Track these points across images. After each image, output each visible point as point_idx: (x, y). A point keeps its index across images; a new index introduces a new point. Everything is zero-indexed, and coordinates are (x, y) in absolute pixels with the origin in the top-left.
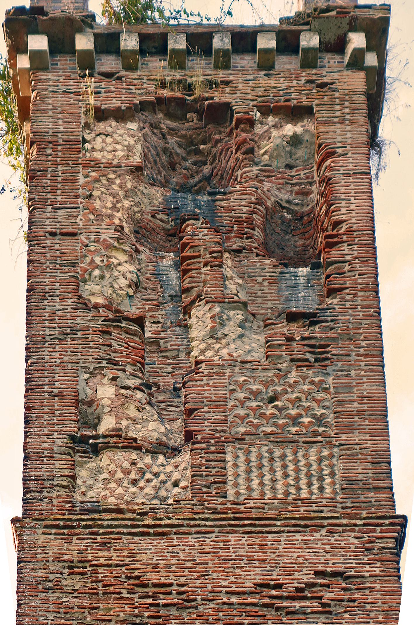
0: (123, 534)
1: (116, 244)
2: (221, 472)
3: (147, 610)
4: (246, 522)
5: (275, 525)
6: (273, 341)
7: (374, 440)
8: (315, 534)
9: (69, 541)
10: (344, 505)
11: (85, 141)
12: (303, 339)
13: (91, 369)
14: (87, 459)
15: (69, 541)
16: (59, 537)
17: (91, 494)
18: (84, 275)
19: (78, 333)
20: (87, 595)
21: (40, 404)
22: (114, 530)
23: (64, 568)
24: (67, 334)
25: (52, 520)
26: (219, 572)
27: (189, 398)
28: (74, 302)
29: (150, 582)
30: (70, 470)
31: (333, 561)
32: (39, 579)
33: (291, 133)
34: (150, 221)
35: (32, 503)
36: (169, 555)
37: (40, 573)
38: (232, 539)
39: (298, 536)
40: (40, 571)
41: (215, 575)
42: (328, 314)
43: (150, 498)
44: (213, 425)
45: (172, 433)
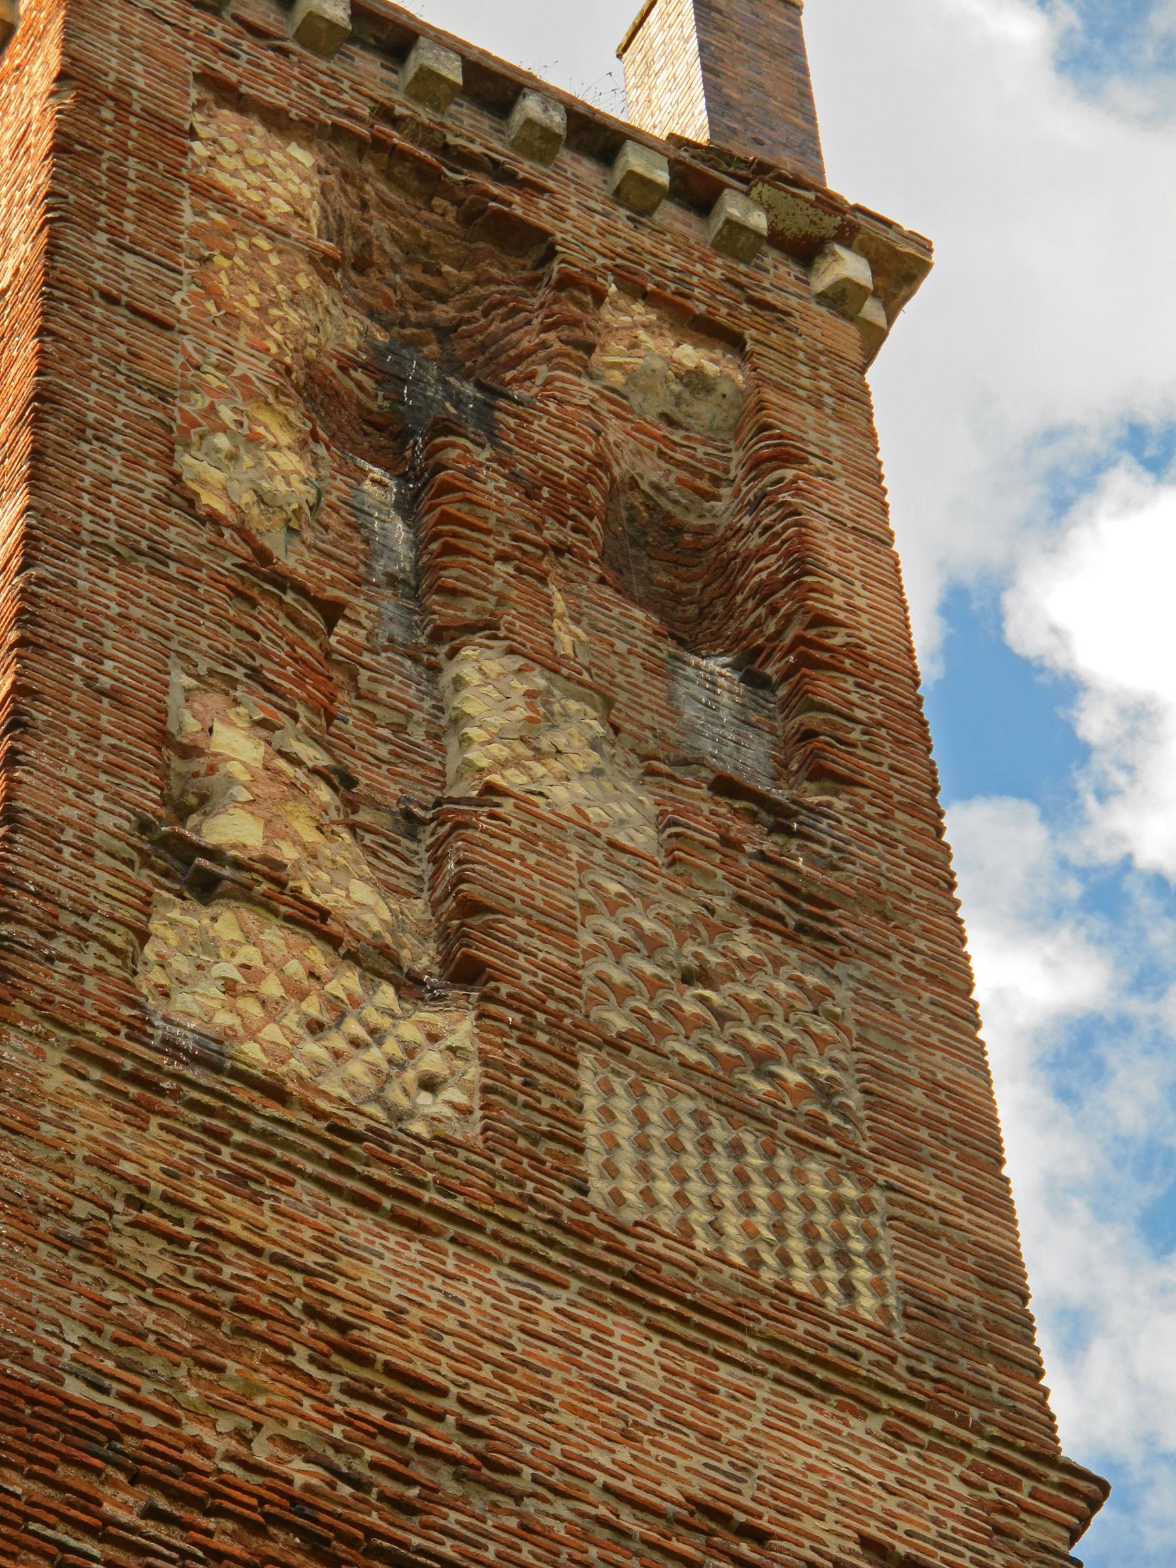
0: (301, 1173)
1: (271, 399)
2: (565, 1112)
3: (372, 1443)
4: (663, 1301)
5: (743, 1346)
6: (689, 827)
7: (980, 1216)
8: (853, 1421)
9: (138, 1122)
10: (913, 1363)
11: (193, 134)
12: (762, 856)
13: (202, 670)
14: (171, 896)
15: (138, 1122)
16: (109, 1097)
17: (183, 1000)
18: (187, 431)
19: (171, 563)
20: (184, 1313)
21: (59, 696)
22: (278, 1152)
23: (114, 1194)
24: (140, 553)
25: (100, 1044)
26: (585, 1415)
27: (473, 871)
28: (163, 484)
29: (381, 1357)
30: (137, 914)
31: (908, 1527)
32: (42, 1198)
33: (690, 364)
34: (333, 374)
35: (23, 956)
36: (436, 1296)
37: (44, 1179)
38: (619, 1331)
39: (803, 1404)
40: (46, 1175)
41: (567, 1419)
42: (823, 826)
43: (363, 1094)
44: (541, 973)
45: (403, 931)
